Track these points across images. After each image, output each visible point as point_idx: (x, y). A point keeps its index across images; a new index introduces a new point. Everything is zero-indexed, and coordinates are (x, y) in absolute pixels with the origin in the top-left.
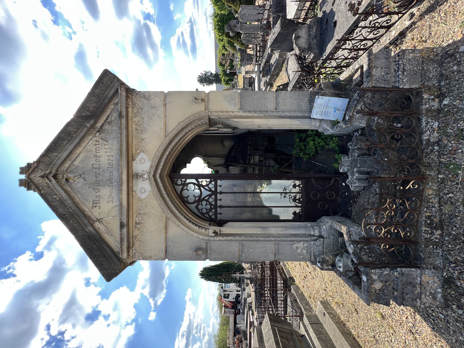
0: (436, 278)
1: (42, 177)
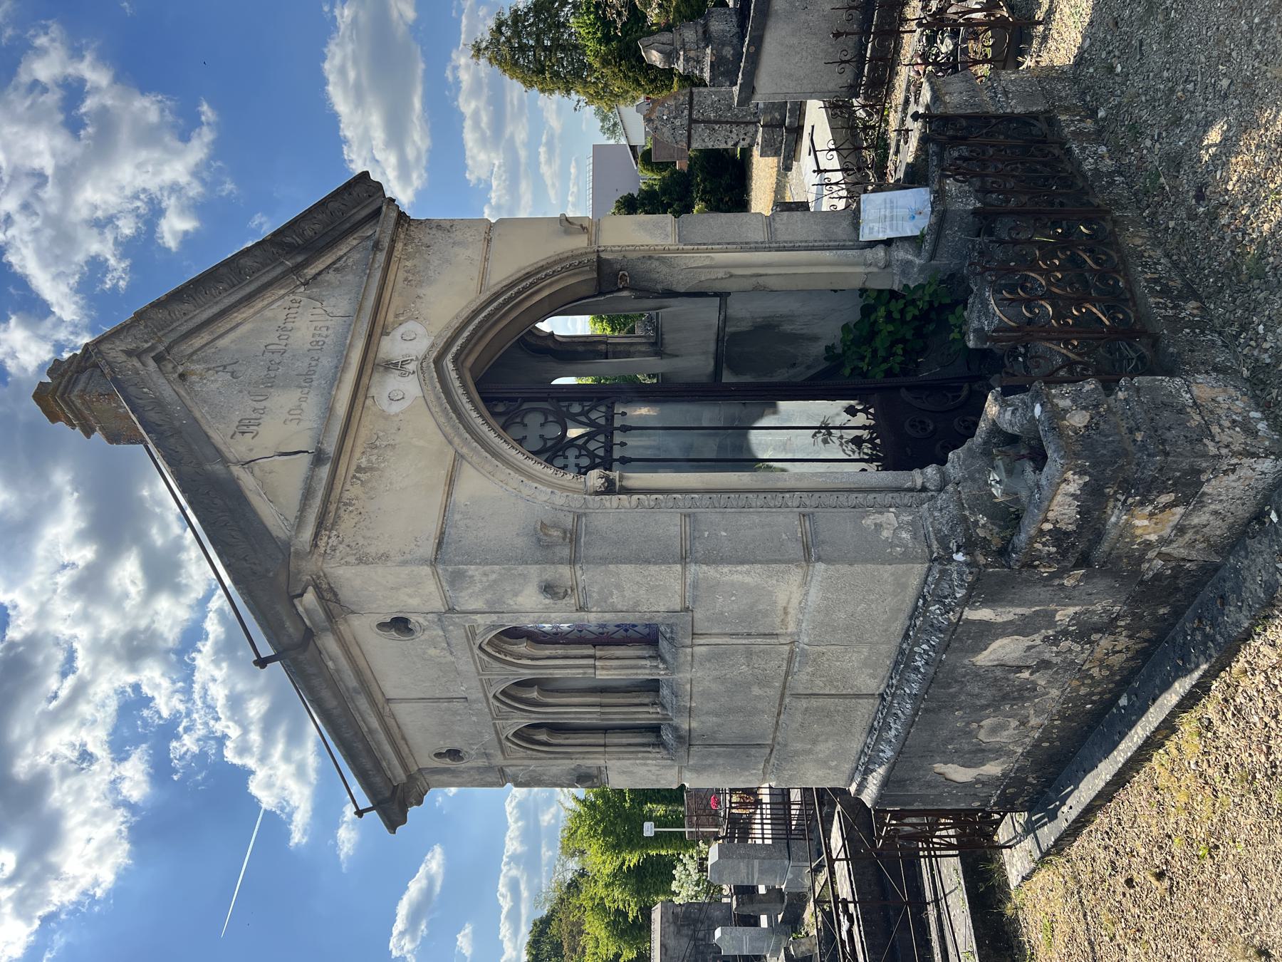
0: (1231, 390)
1: (129, 353)
